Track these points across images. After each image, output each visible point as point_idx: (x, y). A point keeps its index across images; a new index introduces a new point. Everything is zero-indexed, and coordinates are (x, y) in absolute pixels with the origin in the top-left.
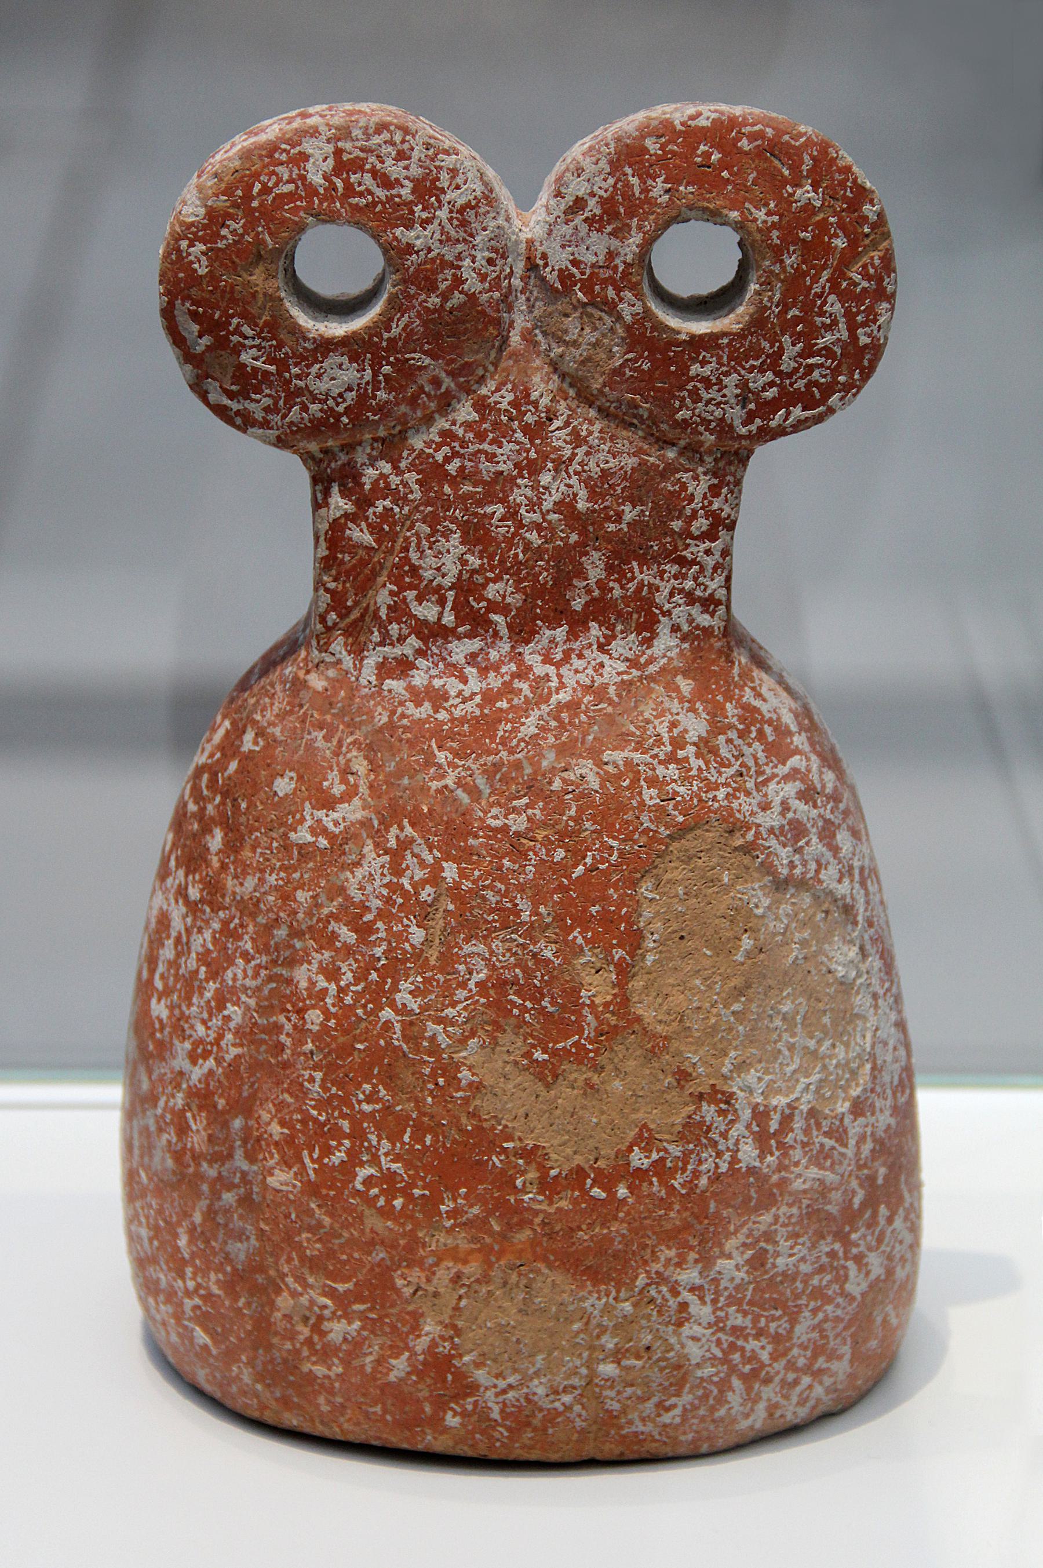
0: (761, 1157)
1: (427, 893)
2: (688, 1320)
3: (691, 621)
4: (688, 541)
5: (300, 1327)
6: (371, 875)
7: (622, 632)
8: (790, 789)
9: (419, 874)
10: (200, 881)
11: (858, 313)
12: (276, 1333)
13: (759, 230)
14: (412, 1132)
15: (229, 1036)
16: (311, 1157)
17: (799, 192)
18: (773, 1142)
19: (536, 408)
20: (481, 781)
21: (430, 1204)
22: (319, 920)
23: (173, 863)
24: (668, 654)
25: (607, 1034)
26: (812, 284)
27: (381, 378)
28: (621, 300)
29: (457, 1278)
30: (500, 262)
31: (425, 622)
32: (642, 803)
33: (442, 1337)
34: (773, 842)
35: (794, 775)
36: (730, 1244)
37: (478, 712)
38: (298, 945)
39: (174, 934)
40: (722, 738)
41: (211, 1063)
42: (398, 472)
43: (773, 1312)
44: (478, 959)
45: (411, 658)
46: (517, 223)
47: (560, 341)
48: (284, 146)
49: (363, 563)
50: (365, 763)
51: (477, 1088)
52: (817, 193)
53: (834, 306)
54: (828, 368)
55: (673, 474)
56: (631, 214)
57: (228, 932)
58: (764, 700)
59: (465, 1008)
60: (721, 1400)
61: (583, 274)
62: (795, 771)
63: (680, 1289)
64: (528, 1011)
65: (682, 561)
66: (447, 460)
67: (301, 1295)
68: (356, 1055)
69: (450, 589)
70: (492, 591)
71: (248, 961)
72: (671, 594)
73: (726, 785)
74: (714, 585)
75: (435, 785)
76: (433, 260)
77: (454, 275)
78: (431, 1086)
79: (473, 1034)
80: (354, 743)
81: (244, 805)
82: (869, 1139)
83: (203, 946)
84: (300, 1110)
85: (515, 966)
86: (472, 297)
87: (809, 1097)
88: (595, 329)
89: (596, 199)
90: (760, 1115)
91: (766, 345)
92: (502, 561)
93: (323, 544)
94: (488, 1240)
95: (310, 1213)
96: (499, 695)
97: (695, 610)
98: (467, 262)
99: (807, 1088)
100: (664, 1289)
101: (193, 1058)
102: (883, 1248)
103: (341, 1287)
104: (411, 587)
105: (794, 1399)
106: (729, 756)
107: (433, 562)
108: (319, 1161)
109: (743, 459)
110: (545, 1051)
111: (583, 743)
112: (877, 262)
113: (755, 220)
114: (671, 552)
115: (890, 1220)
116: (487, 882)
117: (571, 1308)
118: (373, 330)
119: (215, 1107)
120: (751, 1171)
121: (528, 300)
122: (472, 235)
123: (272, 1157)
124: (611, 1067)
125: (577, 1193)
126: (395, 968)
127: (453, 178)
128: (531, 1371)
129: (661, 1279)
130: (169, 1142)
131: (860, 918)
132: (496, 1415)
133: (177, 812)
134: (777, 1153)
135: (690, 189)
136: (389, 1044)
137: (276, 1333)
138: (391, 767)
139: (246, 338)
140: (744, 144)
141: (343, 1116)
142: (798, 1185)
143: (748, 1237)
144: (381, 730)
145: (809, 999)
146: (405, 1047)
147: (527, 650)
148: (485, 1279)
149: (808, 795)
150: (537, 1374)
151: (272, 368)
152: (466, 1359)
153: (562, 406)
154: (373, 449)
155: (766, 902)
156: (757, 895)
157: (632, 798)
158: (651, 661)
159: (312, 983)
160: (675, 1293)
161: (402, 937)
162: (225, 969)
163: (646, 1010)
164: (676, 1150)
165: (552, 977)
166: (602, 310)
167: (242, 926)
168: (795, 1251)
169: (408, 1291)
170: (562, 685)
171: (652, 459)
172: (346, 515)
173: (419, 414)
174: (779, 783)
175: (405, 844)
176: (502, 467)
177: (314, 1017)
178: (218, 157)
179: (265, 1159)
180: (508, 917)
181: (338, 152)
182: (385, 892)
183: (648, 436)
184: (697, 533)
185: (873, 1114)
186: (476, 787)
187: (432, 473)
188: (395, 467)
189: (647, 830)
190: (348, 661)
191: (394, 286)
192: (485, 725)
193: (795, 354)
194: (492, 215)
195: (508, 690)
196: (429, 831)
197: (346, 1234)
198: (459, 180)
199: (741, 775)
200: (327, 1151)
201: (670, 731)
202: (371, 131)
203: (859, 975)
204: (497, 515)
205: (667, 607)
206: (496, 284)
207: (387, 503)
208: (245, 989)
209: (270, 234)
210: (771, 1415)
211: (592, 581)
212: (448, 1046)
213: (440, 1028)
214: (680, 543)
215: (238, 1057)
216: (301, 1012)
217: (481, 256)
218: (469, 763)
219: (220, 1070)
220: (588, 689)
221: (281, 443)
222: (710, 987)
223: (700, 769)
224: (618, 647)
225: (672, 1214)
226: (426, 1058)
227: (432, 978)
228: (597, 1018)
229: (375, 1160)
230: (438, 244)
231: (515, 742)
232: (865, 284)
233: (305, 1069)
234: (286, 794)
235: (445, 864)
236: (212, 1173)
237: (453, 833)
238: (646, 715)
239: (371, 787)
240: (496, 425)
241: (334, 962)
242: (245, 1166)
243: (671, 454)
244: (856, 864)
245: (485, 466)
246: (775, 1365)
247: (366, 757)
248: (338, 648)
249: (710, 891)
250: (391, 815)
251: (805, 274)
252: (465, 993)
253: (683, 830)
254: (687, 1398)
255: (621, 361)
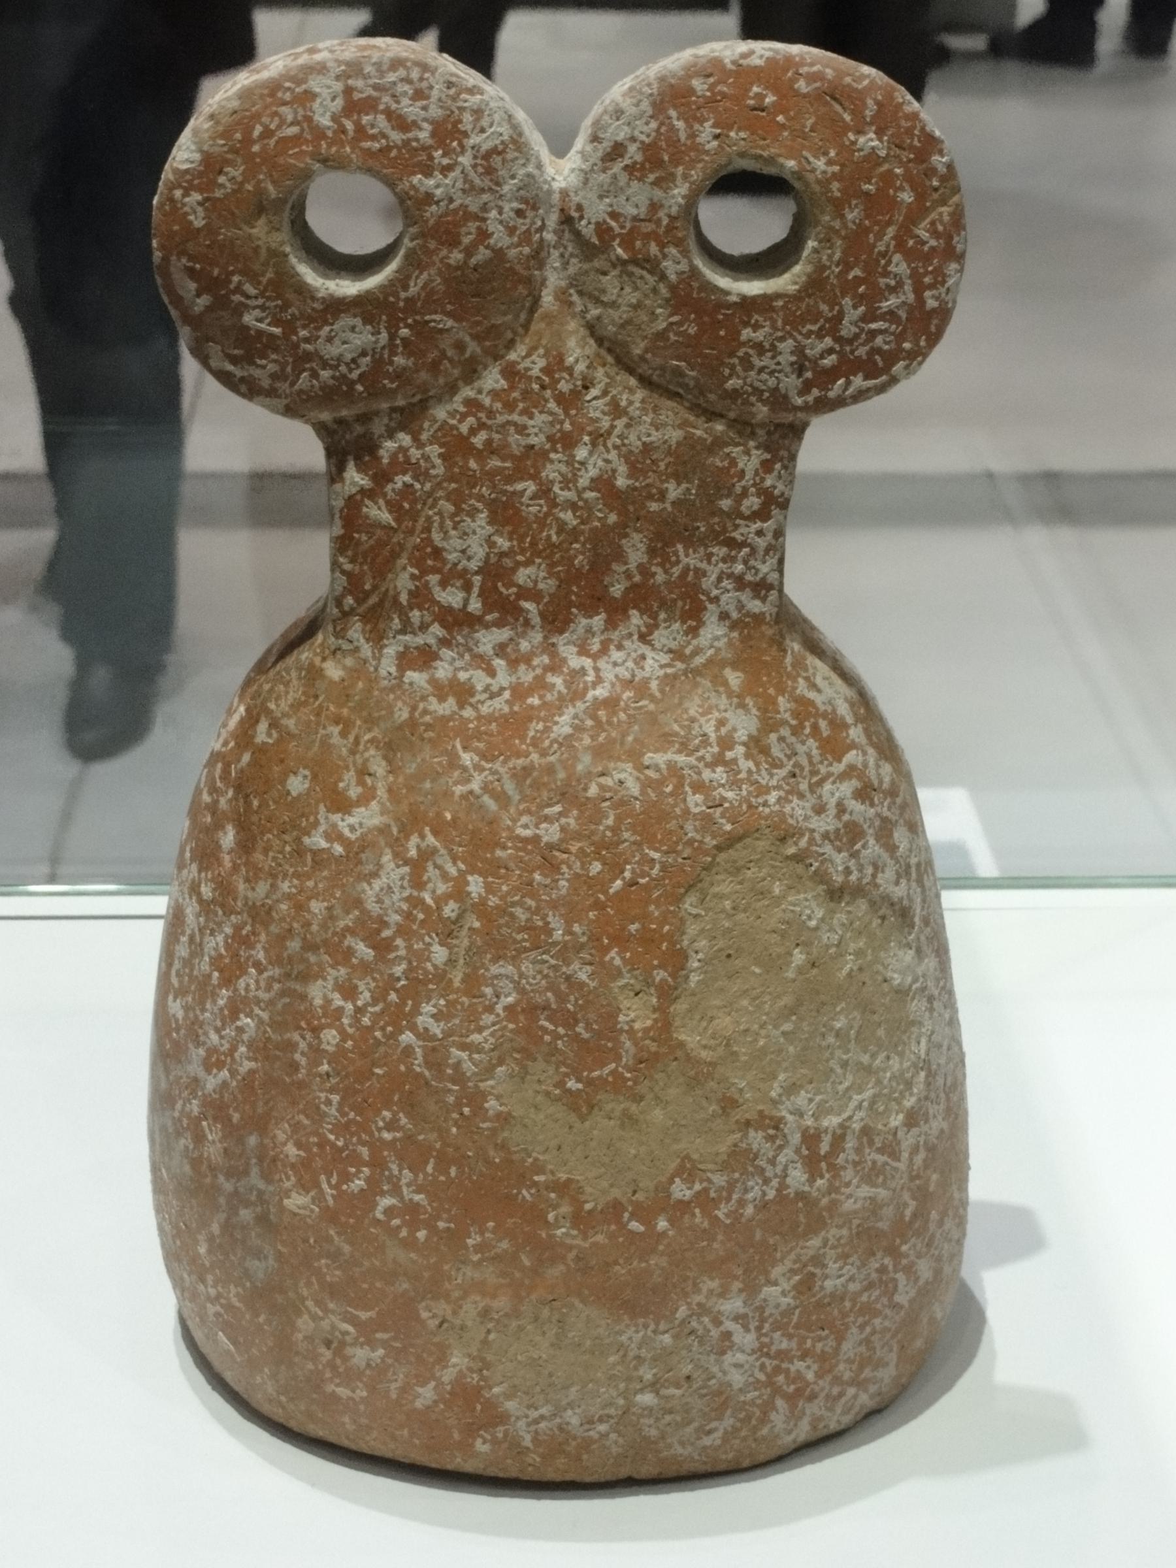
0: (811, 1180)
1: (450, 910)
2: (731, 1348)
3: (740, 607)
4: (738, 521)
5: (322, 1349)
6: (390, 887)
7: (665, 621)
8: (846, 788)
9: (442, 888)
10: (212, 880)
11: (927, 273)
12: (297, 1353)
13: (818, 182)
14: (436, 1164)
15: (243, 1049)
16: (329, 1183)
17: (862, 140)
18: (823, 1165)
19: (571, 375)
20: (510, 787)
21: (456, 1237)
22: (335, 934)
23: (188, 855)
24: (716, 644)
25: (646, 1062)
26: (876, 240)
27: (398, 342)
28: (665, 256)
29: (485, 1313)
30: (530, 214)
31: (449, 610)
32: (687, 812)
33: (470, 1370)
34: (828, 849)
35: (850, 771)
36: (777, 1272)
37: (506, 709)
38: (313, 959)
39: (188, 932)
40: (773, 737)
41: (225, 1074)
42: (420, 445)
43: (820, 1332)
44: (507, 981)
45: (435, 648)
46: (550, 171)
47: (598, 301)
48: (287, 84)
49: (381, 544)
50: (384, 763)
51: (504, 1119)
52: (880, 140)
53: (900, 266)
54: (893, 334)
55: (721, 448)
56: (676, 162)
57: (240, 940)
58: (819, 691)
59: (492, 1034)
60: (764, 1420)
61: (622, 227)
62: (851, 768)
63: (723, 1319)
64: (560, 1037)
65: (732, 543)
66: (473, 431)
67: (322, 1319)
68: (376, 1080)
69: (477, 573)
70: (523, 576)
71: (260, 972)
72: (720, 579)
73: (778, 788)
74: (765, 568)
75: (459, 790)
76: (456, 211)
77: (479, 228)
78: (455, 1116)
79: (501, 1062)
80: (372, 741)
81: (256, 803)
82: (922, 1149)
83: (216, 949)
84: (316, 1133)
85: (547, 989)
86: (499, 253)
87: (861, 1114)
88: (636, 289)
89: (638, 144)
90: (811, 1138)
91: (824, 308)
92: (533, 544)
93: (338, 522)
94: (518, 1275)
95: (329, 1239)
96: (530, 691)
97: (745, 596)
98: (493, 214)
99: (859, 1107)
100: (706, 1320)
101: (208, 1066)
102: (933, 1251)
103: (364, 1315)
104: (435, 570)
105: (839, 1410)
106: (781, 756)
107: (457, 543)
108: (337, 1187)
109: (797, 431)
110: (579, 1080)
111: (622, 744)
112: (946, 218)
113: (813, 171)
114: (718, 534)
115: (941, 1223)
116: (516, 898)
117: (607, 1341)
118: (389, 288)
119: (230, 1120)
120: (801, 1196)
121: (562, 255)
122: (498, 184)
123: (288, 1179)
124: (651, 1096)
125: (613, 1227)
126: (418, 986)
127: (477, 120)
128: (564, 1403)
129: (703, 1310)
130: (186, 1147)
131: (917, 920)
132: (527, 1441)
133: (193, 802)
134: (827, 1176)
135: (742, 135)
136: (410, 1069)
137: (297, 1353)
138: (411, 768)
139: (248, 297)
140: (802, 85)
141: (364, 1144)
142: (849, 1205)
143: (795, 1262)
144: (400, 728)
145: (863, 1013)
146: (427, 1073)
147: (560, 640)
148: (516, 1313)
149: (865, 793)
150: (570, 1405)
151: (277, 331)
152: (496, 1390)
153: (600, 373)
154: (391, 419)
155: (819, 913)
156: (811, 908)
157: (676, 805)
158: (697, 652)
159: (328, 1001)
160: (717, 1322)
161: (424, 956)
162: (238, 978)
163: (689, 1037)
164: (719, 1180)
165: (587, 1002)
166: (643, 268)
167: (254, 933)
168: (844, 1271)
169: (433, 1324)
170: (599, 680)
171: (698, 433)
172: (362, 491)
173: (441, 381)
174: (834, 783)
175: (427, 855)
176: (533, 440)
177: (330, 1037)
178: (217, 98)
179: (281, 1180)
180: (539, 936)
181: (348, 91)
182: (405, 907)
183: (695, 408)
184: (747, 513)
185: (926, 1121)
186: (504, 792)
187: (456, 447)
188: (416, 439)
189: (690, 842)
190: (366, 650)
191: (412, 240)
192: (515, 723)
193: (855, 318)
194: (522, 161)
195: (540, 684)
196: (452, 841)
197: (366, 1263)
198: (484, 123)
199: (794, 776)
200: (346, 1178)
201: (717, 729)
202: (385, 67)
203: (915, 980)
204: (528, 493)
205: (715, 592)
206: (526, 238)
207: (407, 478)
208: (258, 1002)
209: (273, 182)
210: (815, 1428)
211: (632, 566)
212: (474, 1074)
213: (464, 1055)
214: (729, 525)
215: (252, 1072)
216: (316, 1031)
217: (509, 207)
218: (497, 766)
219: (234, 1083)
220: (628, 683)
221: (290, 411)
222: (758, 1007)
223: (750, 772)
224: (661, 637)
225: (715, 1245)
226: (450, 1085)
227: (456, 1001)
228: (636, 1044)
229: (396, 1191)
230: (460, 193)
231: (547, 743)
232: (933, 243)
233: (321, 1091)
234: (300, 795)
235: (470, 878)
236: (228, 1187)
237: (480, 844)
238: (692, 712)
239: (390, 791)
240: (526, 394)
241: (350, 980)
242: (261, 1185)
243: (719, 427)
244: (913, 861)
245: (514, 438)
246: (821, 1382)
247: (385, 757)
248: (356, 635)
249: (760, 904)
250: (412, 822)
251: (867, 231)
252: (492, 1018)
253: (730, 842)
254: (728, 1422)
255: (664, 325)
